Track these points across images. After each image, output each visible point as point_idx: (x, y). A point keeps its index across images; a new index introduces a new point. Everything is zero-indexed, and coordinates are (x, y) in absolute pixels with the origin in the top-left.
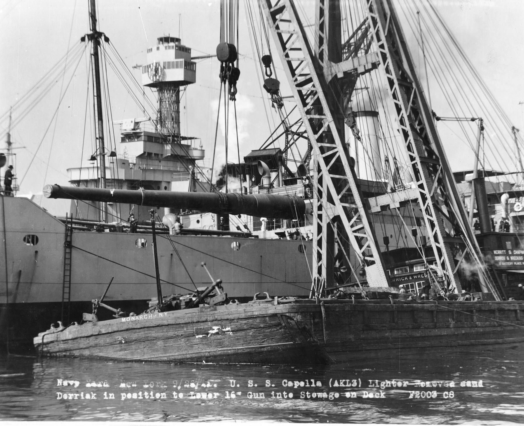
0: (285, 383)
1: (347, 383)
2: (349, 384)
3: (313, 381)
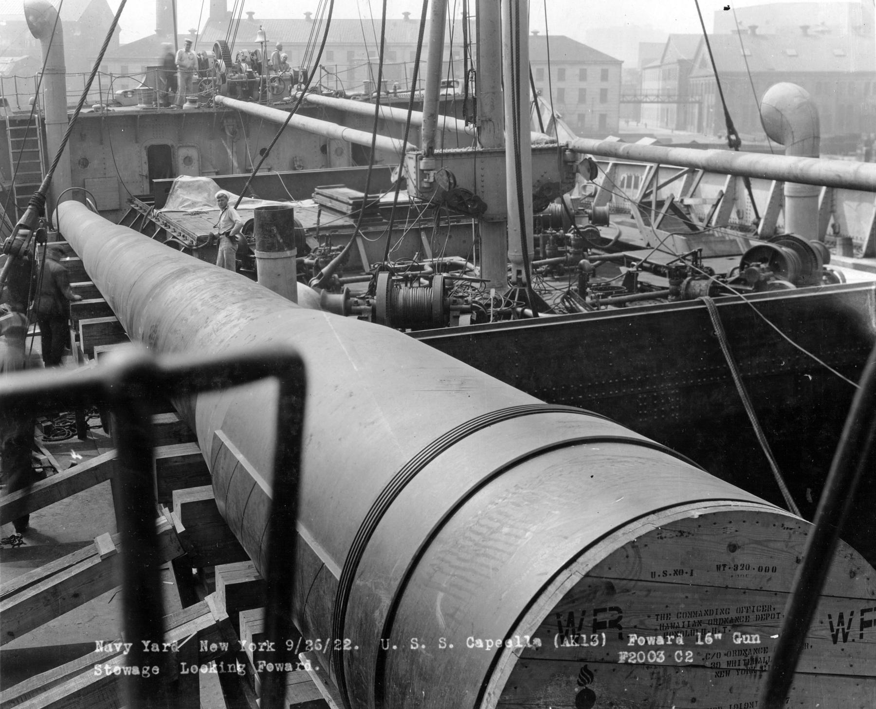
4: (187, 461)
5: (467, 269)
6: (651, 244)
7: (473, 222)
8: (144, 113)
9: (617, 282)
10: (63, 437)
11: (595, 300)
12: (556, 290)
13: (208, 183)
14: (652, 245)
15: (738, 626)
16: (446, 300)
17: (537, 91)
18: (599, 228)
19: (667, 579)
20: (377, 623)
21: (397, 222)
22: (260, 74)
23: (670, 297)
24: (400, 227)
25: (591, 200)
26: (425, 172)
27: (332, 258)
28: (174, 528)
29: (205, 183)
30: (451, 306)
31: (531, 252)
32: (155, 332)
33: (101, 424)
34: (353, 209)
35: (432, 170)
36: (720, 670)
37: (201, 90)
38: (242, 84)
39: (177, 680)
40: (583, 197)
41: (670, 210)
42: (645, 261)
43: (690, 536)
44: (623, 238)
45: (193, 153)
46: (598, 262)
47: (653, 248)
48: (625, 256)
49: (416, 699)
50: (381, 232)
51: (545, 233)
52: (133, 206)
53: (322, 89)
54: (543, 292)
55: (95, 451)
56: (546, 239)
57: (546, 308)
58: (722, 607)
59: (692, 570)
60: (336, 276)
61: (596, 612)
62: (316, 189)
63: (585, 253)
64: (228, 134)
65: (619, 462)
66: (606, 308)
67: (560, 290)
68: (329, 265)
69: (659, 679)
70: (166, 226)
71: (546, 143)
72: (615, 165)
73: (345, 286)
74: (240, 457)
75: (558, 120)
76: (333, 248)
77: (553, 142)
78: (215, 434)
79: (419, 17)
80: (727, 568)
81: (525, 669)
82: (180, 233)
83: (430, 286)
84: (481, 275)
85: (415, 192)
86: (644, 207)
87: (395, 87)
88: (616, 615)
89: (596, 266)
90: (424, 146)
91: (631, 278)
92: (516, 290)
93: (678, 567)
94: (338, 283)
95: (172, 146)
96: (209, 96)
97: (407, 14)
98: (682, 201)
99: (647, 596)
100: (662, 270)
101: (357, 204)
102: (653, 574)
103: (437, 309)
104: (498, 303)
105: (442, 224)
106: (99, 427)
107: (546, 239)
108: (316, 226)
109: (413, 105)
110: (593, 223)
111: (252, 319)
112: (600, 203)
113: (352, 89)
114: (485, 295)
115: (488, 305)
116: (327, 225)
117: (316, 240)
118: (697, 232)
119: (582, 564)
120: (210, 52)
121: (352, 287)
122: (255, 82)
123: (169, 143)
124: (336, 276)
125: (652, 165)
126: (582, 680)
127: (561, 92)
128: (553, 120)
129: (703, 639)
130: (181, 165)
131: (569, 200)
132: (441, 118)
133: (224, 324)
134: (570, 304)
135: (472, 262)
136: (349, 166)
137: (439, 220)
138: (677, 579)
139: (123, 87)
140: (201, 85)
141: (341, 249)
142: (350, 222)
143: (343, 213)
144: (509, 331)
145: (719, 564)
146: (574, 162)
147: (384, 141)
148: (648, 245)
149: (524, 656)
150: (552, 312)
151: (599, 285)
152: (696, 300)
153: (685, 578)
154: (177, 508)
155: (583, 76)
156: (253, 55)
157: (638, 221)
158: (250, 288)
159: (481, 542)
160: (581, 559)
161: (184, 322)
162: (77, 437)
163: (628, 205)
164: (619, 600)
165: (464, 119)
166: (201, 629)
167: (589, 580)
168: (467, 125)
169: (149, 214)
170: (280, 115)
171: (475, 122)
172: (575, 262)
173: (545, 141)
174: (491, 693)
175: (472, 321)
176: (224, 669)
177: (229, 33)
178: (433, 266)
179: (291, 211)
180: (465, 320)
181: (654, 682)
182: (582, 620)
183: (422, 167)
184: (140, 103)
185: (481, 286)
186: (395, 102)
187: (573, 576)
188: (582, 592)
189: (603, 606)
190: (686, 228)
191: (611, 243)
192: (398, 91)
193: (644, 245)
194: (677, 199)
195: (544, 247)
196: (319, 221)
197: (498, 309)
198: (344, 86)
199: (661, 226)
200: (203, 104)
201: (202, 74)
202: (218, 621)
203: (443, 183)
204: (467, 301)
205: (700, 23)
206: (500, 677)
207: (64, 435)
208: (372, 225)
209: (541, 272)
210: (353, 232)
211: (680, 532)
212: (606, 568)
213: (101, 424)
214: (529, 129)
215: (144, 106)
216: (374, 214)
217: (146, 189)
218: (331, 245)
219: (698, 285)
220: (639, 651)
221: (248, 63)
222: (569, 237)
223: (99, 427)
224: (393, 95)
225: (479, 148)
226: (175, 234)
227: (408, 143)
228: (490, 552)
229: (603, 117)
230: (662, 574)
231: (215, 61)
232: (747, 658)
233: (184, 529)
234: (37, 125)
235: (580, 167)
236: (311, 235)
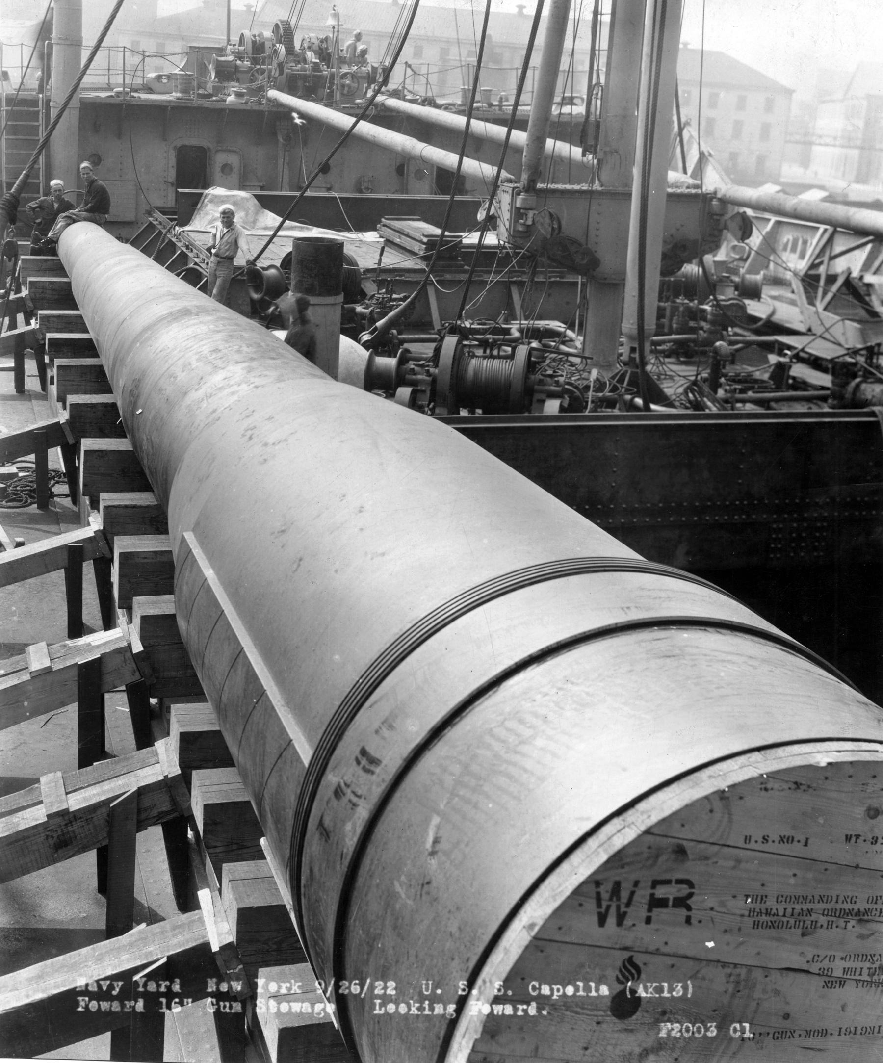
0: (534, 988)
1: (377, 1007)
2: (380, 1009)
3: (593, 984)
4: (159, 559)
5: (567, 339)
6: (813, 329)
7: (579, 279)
8: (177, 104)
9: (762, 374)
10: (18, 504)
11: (729, 395)
12: (680, 376)
13: (247, 199)
14: (814, 330)
15: (868, 921)
16: (529, 378)
17: (683, 120)
18: (747, 302)
19: (768, 847)
20: (347, 840)
21: (482, 271)
22: (328, 67)
23: (830, 401)
24: (485, 277)
25: (741, 264)
26: (522, 211)
27: (391, 309)
28: (129, 646)
29: (243, 199)
30: (536, 387)
31: (651, 323)
32: (137, 387)
33: (68, 493)
34: (427, 250)
35: (531, 209)
36: (831, 979)
37: (252, 81)
38: (305, 78)
39: (106, 846)
40: (731, 260)
41: (844, 289)
42: (803, 350)
43: (811, 790)
44: (776, 318)
45: (233, 160)
46: (740, 346)
47: (814, 335)
48: (777, 341)
49: (386, 959)
50: (460, 281)
51: (674, 302)
52: (151, 219)
53: (406, 92)
54: (663, 377)
55: (57, 527)
56: (675, 309)
57: (662, 399)
58: (846, 894)
59: (807, 839)
60: (395, 332)
61: (655, 884)
62: (383, 220)
63: (725, 333)
64: (281, 140)
65: (718, 661)
66: (744, 406)
67: (684, 377)
68: (386, 318)
69: (738, 982)
70: (187, 248)
71: (688, 188)
72: (778, 223)
73: (406, 346)
74: (209, 573)
75: (710, 159)
76: (395, 296)
77: (696, 187)
78: (183, 537)
79: (533, 12)
80: (860, 840)
81: (539, 954)
82: (204, 260)
83: (512, 357)
84: (583, 349)
85: (506, 236)
86: (810, 281)
87: (501, 98)
88: (684, 890)
89: (737, 350)
90: (525, 177)
91: (781, 370)
92: (626, 372)
93: (787, 832)
94: (396, 341)
95: (209, 149)
96: (261, 89)
97: (521, 8)
98: (861, 278)
99: (734, 868)
100: (824, 363)
101: (432, 244)
102: (748, 839)
103: (518, 385)
104: (600, 386)
105: (540, 278)
106: (67, 496)
107: (675, 309)
108: (376, 266)
109: (514, 122)
110: (739, 295)
111: (256, 387)
112: (753, 270)
113: (443, 96)
114: (585, 375)
115: (587, 388)
116: (392, 267)
117: (375, 285)
118: (878, 319)
119: (642, 813)
120: (268, 34)
121: (414, 348)
122: (321, 77)
123: (205, 144)
124: (395, 332)
125: (828, 227)
126: (623, 975)
127: (711, 122)
128: (703, 158)
130: (218, 175)
131: (711, 263)
132: (550, 143)
133: (220, 389)
134: (694, 396)
135: (573, 330)
136: (431, 194)
137: (534, 273)
138: (785, 848)
139: (157, 69)
140: (253, 75)
141: (404, 299)
142: (421, 265)
143: (413, 253)
144: (610, 426)
145: (849, 833)
146: (722, 215)
147: (471, 165)
148: (810, 330)
149: (539, 936)
150: (670, 405)
151: (738, 375)
152: (865, 410)
153: (796, 849)
154: (137, 621)
155: (741, 104)
156: (322, 41)
157: (800, 297)
158: (263, 344)
159: (502, 753)
160: (642, 806)
161: (172, 379)
162: (35, 506)
163: (789, 275)
164: (691, 870)
165: (581, 147)
166: (143, 784)
167: (649, 838)
168: (584, 155)
169: (169, 231)
170: (343, 120)
171: (595, 152)
172: (709, 343)
173: (686, 185)
174: (487, 980)
175: (562, 409)
176: (429, 1010)
177: (292, 13)
178: (521, 330)
179: (341, 245)
180: (552, 407)
181: (731, 988)
182: (633, 893)
183: (518, 205)
184: (176, 92)
185: (582, 362)
186: (496, 117)
187: (627, 829)
188: (637, 854)
189: (667, 876)
190: (862, 313)
191: (760, 323)
192: (504, 103)
193: (802, 328)
194: (855, 274)
195: (671, 320)
196: (380, 260)
197: (601, 395)
198: (434, 91)
199: (829, 307)
200: (253, 99)
201: (255, 61)
202: (166, 777)
203: (544, 229)
204: (557, 382)
206: (503, 959)
207: (20, 501)
208: (450, 272)
209: (663, 351)
210: (421, 278)
211: (796, 783)
212: (677, 825)
213: (68, 493)
214: (669, 164)
215: (179, 95)
216: (454, 258)
217: (171, 202)
218: (393, 292)
219: (869, 390)
221: (315, 52)
222: (704, 311)
223: (67, 496)
224: (497, 108)
225: (597, 186)
226: (196, 260)
227: (502, 171)
228: (512, 770)
229: (761, 160)
230: (760, 840)
231: (274, 45)
232: (874, 966)
233: (141, 649)
234: (40, 108)
235: (729, 223)
236: (369, 278)
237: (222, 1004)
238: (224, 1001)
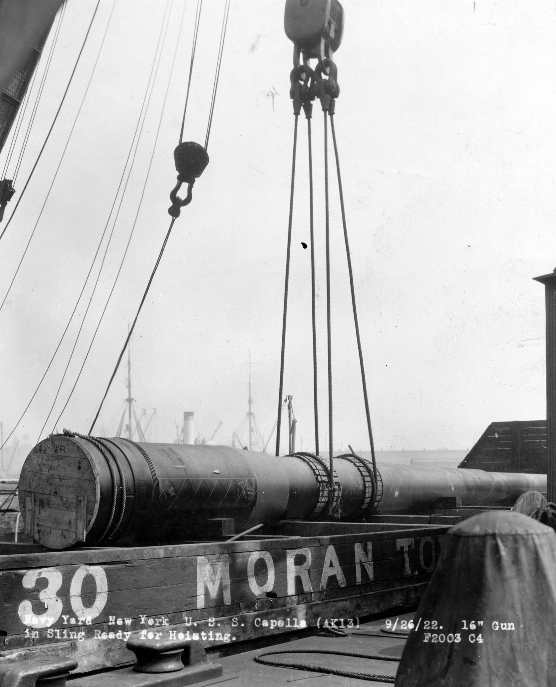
0: (472, 638)
106: (367, 482)
129: (468, 626)
176: (213, 637)
205: (33, 166)
220: (440, 634)
237: (502, 624)
238: (503, 622)
